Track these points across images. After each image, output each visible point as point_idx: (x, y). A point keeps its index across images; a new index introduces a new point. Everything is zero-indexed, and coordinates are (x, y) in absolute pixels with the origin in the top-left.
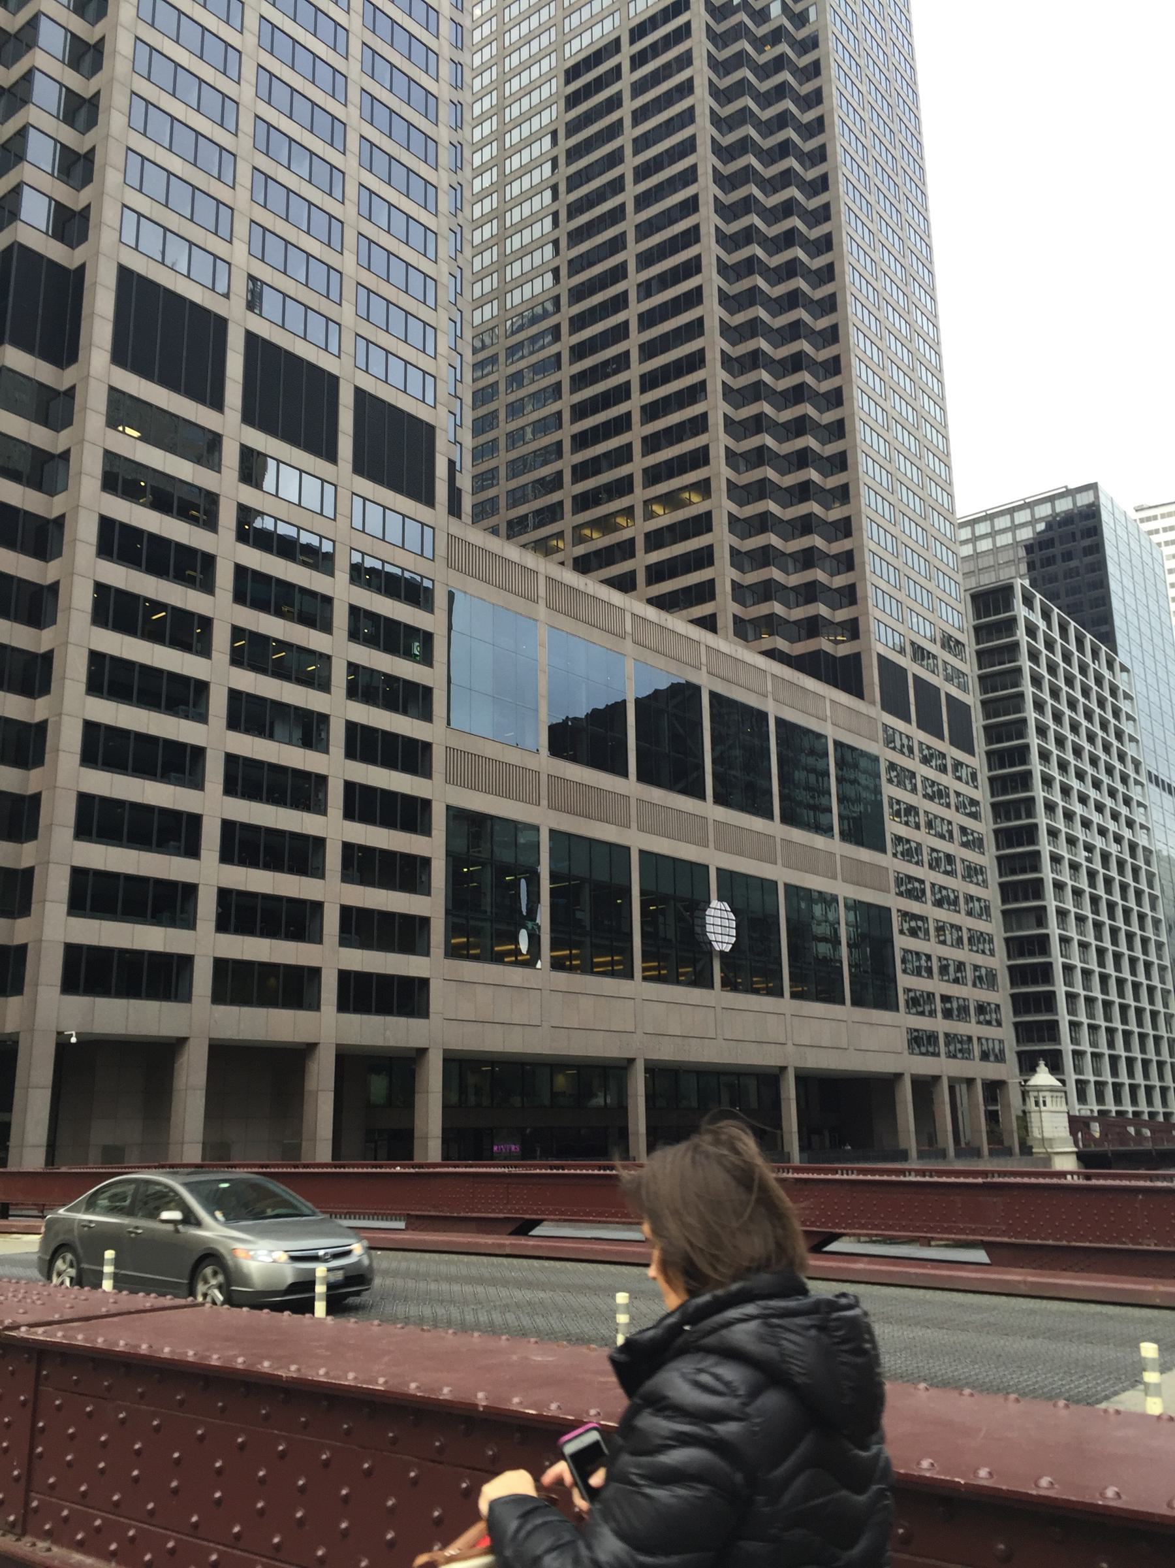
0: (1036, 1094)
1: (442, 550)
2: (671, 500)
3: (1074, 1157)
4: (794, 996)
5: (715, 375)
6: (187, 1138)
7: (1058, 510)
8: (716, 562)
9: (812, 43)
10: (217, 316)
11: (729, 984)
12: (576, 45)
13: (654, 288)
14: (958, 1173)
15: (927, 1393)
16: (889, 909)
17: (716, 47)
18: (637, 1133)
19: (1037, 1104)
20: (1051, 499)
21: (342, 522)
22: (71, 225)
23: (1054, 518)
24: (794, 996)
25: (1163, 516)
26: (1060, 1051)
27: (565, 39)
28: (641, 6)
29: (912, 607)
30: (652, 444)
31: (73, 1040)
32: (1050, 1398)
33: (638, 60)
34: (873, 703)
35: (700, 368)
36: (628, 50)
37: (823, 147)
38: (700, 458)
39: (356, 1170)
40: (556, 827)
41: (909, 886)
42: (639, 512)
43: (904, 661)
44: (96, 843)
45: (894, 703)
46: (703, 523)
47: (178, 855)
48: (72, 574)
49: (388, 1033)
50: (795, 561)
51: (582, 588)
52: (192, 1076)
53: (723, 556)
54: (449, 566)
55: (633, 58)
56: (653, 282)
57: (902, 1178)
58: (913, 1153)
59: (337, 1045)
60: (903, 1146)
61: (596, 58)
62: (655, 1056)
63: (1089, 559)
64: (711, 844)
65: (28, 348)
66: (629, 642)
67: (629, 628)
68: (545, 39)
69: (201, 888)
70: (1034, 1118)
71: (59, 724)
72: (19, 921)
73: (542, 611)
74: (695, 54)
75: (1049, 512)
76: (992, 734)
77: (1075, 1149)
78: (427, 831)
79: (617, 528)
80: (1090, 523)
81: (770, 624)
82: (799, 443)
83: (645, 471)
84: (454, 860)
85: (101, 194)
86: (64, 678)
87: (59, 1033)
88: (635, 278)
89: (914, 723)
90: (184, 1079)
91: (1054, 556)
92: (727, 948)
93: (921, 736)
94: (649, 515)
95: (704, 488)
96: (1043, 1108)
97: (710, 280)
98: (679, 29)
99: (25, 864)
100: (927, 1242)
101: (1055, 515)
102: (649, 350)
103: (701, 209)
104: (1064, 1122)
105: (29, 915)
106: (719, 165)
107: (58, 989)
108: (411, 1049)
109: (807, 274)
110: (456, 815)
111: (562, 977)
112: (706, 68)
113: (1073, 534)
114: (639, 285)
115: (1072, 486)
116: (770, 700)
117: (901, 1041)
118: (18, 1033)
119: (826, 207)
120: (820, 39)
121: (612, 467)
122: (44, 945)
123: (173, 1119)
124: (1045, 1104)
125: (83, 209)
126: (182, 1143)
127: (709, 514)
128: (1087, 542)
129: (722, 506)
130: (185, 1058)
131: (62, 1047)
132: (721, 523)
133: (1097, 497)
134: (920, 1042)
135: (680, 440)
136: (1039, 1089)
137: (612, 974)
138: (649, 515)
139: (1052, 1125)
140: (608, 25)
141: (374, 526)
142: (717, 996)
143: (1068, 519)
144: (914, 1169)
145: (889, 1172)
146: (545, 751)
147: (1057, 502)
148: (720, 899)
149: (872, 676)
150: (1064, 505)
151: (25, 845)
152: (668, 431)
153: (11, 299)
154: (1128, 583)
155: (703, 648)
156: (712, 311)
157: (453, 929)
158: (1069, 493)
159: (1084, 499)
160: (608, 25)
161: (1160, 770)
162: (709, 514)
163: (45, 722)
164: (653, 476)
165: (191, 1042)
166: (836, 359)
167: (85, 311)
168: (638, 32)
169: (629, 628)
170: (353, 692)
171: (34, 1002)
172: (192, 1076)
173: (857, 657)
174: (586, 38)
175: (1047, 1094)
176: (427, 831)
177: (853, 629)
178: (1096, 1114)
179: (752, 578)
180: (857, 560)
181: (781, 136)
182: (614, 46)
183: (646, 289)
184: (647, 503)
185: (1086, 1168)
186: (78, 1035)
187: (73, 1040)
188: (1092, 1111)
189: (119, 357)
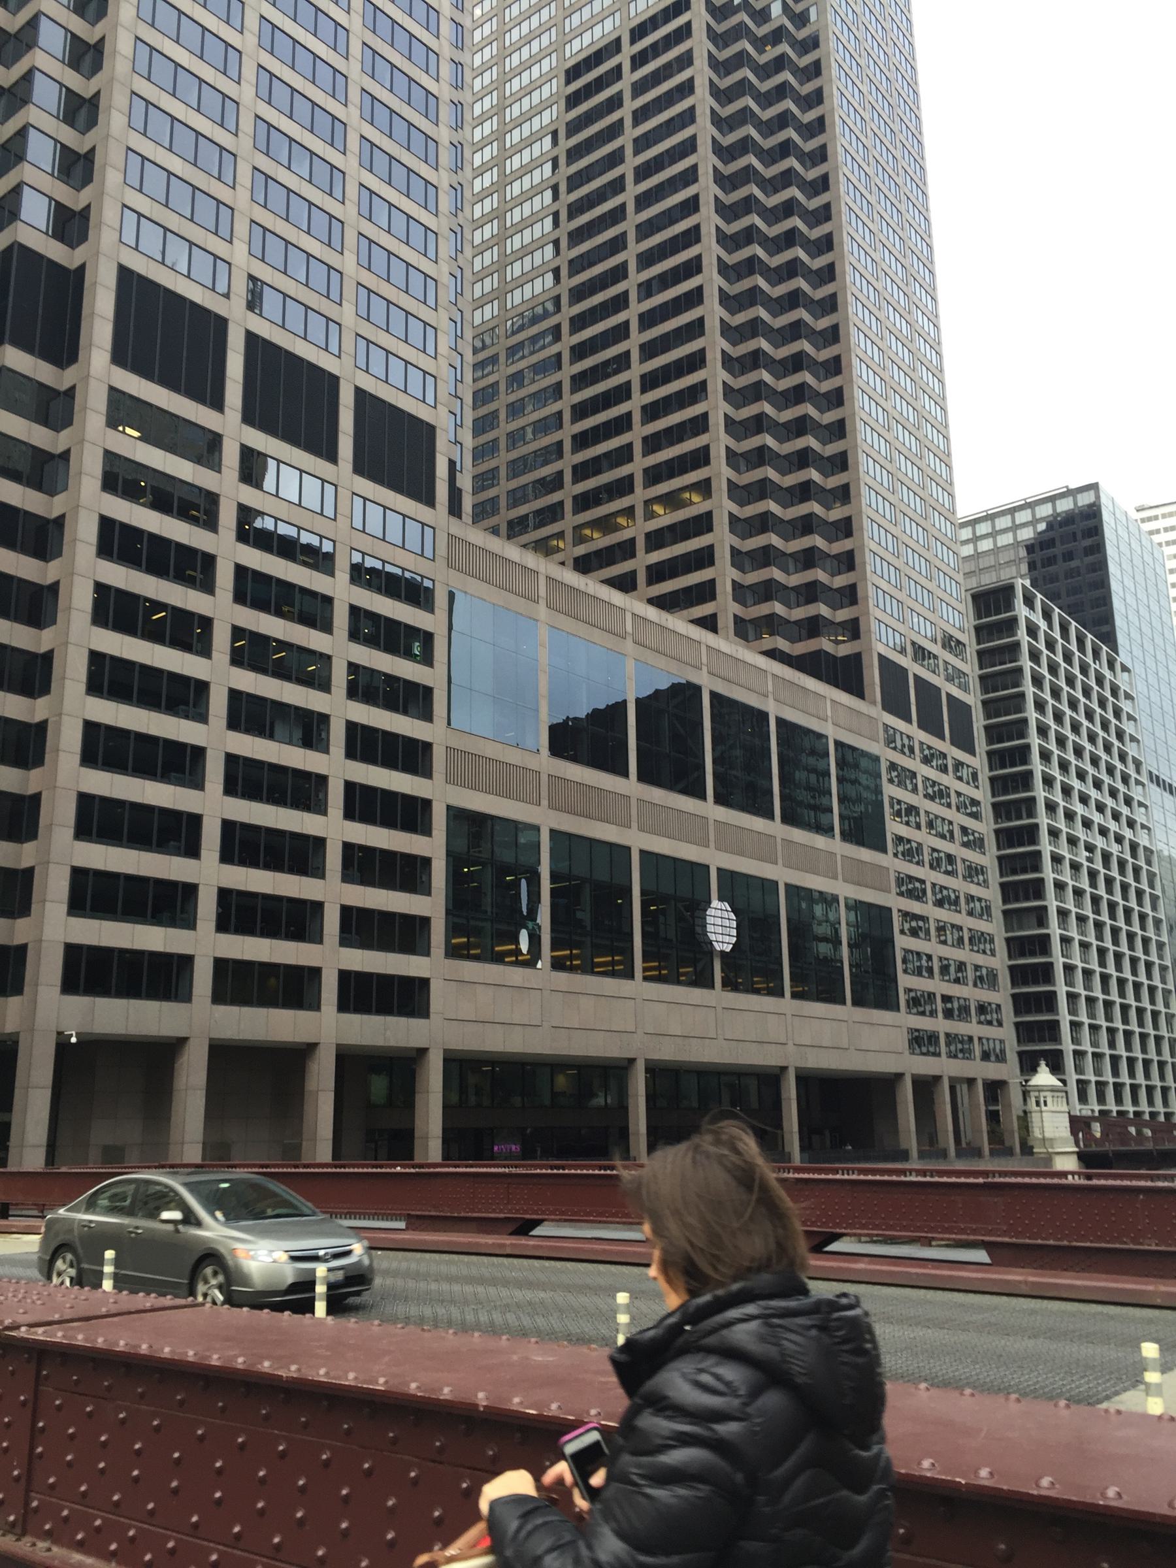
0: (1036, 1094)
1: (442, 550)
2: (672, 500)
3: (1075, 1157)
4: (795, 996)
5: (715, 375)
6: (187, 1138)
7: (1059, 510)
8: (716, 562)
9: (813, 43)
10: (217, 316)
11: (730, 984)
12: (576, 45)
13: (654, 288)
14: (959, 1173)
15: (928, 1393)
16: (890, 909)
17: (717, 47)
18: (637, 1133)
19: (1038, 1104)
20: (1052, 499)
21: (342, 522)
22: (71, 225)
23: (1055, 518)
24: (795, 996)
25: (1164, 516)
26: (1061, 1051)
27: (566, 39)
28: (641, 6)
29: (913, 607)
30: (652, 444)
31: (74, 1040)
32: (1051, 1398)
33: (639, 60)
34: (874, 703)
35: (701, 368)
36: (628, 50)
37: (823, 147)
38: (701, 458)
39: (356, 1170)
40: (556, 827)
41: (910, 886)
42: (639, 512)
43: (905, 661)
44: (96, 843)
45: (895, 703)
46: (703, 523)
47: (178, 855)
48: (73, 574)
49: (388, 1033)
50: (796, 561)
51: (582, 588)
52: (192, 1076)
53: (723, 556)
54: (450, 566)
55: (633, 58)
56: (654, 282)
57: (903, 1178)
58: (914, 1153)
59: (338, 1045)
60: (903, 1146)
61: (597, 58)
62: (656, 1056)
63: (1090, 559)
64: (712, 844)
65: (28, 348)
66: (629, 642)
67: (629, 628)
68: (545, 39)
69: (201, 888)
70: (1035, 1118)
71: (59, 724)
72: (19, 921)
73: (542, 611)
74: (695, 54)
75: (1050, 512)
76: (993, 734)
77: (1076, 1149)
78: (427, 831)
79: (617, 528)
80: (1091, 523)
81: (771, 624)
82: (800, 443)
83: (646, 471)
84: (455, 860)
85: (101, 194)
86: (64, 678)
87: (59, 1033)
88: (635, 278)
89: (915, 723)
90: (184, 1079)
91: (1055, 556)
92: (728, 948)
93: (922, 736)
94: (650, 515)
95: (704, 488)
96: (1044, 1108)
97: (711, 280)
98: (680, 29)
99: (25, 864)
100: (928, 1242)
101: (1055, 515)
102: (649, 350)
103: (701, 209)
104: (1065, 1122)
105: (29, 915)
106: (719, 165)
107: (58, 989)
108: (412, 1049)
109: (808, 274)
110: (456, 815)
111: (562, 977)
112: (707, 68)
113: (1074, 534)
114: (639, 285)
115: (1073, 486)
116: (771, 700)
117: (901, 1041)
118: (18, 1033)
119: (827, 207)
120: (821, 39)
121: (612, 467)
122: (44, 945)
123: (173, 1119)
124: (1046, 1104)
125: (83, 209)
126: (183, 1143)
127: (709, 514)
128: (1087, 542)
129: (723, 506)
130: (185, 1058)
131: (63, 1047)
132: (721, 523)
133: (1098, 497)
134: (921, 1042)
135: (681, 440)
136: (1040, 1089)
137: (613, 974)
138: (650, 515)
139: (1052, 1125)
140: (608, 25)
141: (374, 526)
142: (718, 996)
143: (1069, 519)
144: (914, 1169)
145: (890, 1172)
146: (545, 751)
147: (1058, 502)
148: (721, 899)
149: (873, 676)
150: (1065, 505)
151: (25, 845)
152: (668, 431)
153: (11, 299)
154: (1128, 583)
155: (704, 648)
156: (713, 311)
157: (453, 929)
158: (1070, 493)
159: (1085, 499)
160: (608, 25)
161: (1161, 770)
162: (709, 514)
163: (45, 722)
164: (654, 476)
165: (191, 1042)
166: (837, 359)
167: (85, 311)
168: (639, 32)
169: (629, 628)
170: (353, 692)
171: (34, 1002)
172: (192, 1076)
173: (857, 657)
174: (587, 38)
175: (1048, 1094)
176: (427, 831)
177: (853, 629)
178: (1097, 1114)
179: (753, 578)
180: (857, 560)
181: (781, 136)
182: (615, 46)
183: (647, 289)
184: (648, 503)
185: (1087, 1168)
186: (78, 1035)
187: (74, 1040)
188: (1093, 1111)
189: (119, 357)
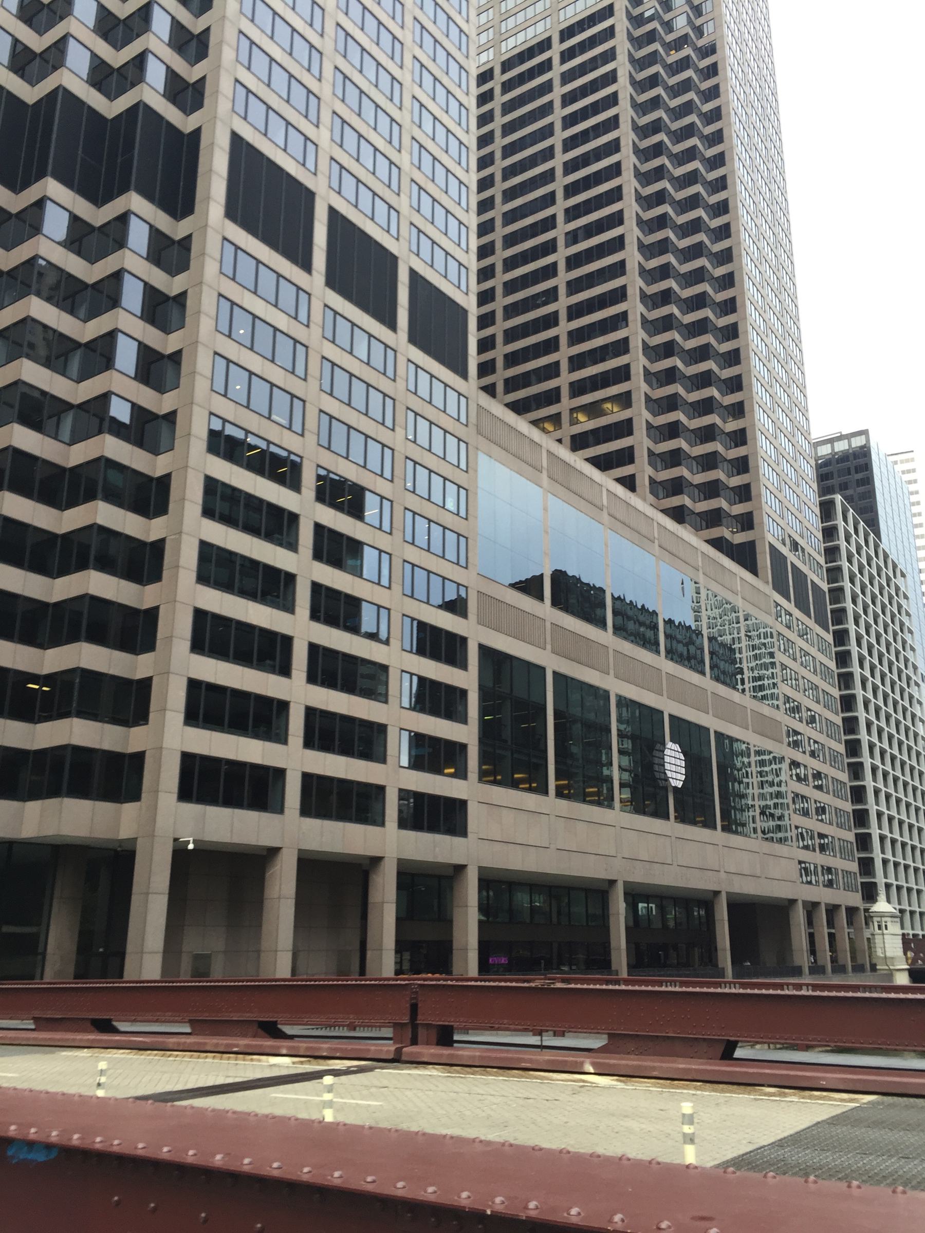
0: (879, 919)
2: (593, 410)
5: (634, 307)
6: (280, 947)
7: (836, 450)
8: (636, 460)
9: (711, 50)
10: (307, 189)
11: (682, 818)
12: (511, 42)
13: (580, 236)
14: (856, 988)
15: (905, 1196)
18: (619, 949)
19: (880, 928)
20: (831, 441)
21: (401, 383)
22: (188, 94)
23: (833, 456)
25: (902, 462)
26: (875, 884)
28: (580, 6)
29: (787, 507)
30: (577, 362)
31: (191, 846)
32: (846, 1177)
33: (567, 56)
35: (622, 302)
36: (557, 48)
37: (720, 131)
39: (509, 984)
40: (557, 670)
41: (795, 738)
42: (565, 418)
43: (785, 551)
44: (209, 656)
45: (780, 586)
47: (273, 672)
48: (192, 403)
49: (437, 849)
51: (572, 463)
52: (283, 883)
53: (641, 456)
55: (503, 84)
56: (579, 232)
57: (779, 992)
59: (399, 860)
60: (797, 962)
62: (631, 879)
63: (861, 489)
66: (605, 514)
69: (292, 705)
70: (878, 939)
71: (178, 543)
72: (135, 730)
75: (830, 451)
77: (907, 967)
79: (602, 413)
80: (861, 461)
82: (703, 367)
83: (572, 384)
87: (176, 840)
88: (562, 228)
89: (793, 602)
90: (277, 888)
91: (833, 486)
92: (679, 784)
94: (574, 422)
95: (625, 400)
96: (885, 932)
97: (631, 231)
98: (542, 63)
100: (807, 1048)
101: (834, 454)
103: (623, 173)
104: (899, 942)
105: (147, 724)
107: (175, 796)
108: (449, 865)
110: (486, 652)
111: (563, 803)
112: (627, 63)
113: (849, 469)
114: (567, 234)
117: (793, 870)
118: (135, 840)
119: (724, 178)
120: (718, 47)
121: (540, 381)
123: (264, 927)
124: (886, 929)
125: (197, 81)
126: (276, 951)
127: (630, 421)
128: (860, 476)
129: (641, 415)
130: (278, 867)
131: (180, 854)
133: (868, 440)
135: (603, 360)
136: (882, 915)
137: (599, 803)
138: (574, 422)
139: (890, 946)
140: (540, 27)
141: (423, 391)
142: (670, 827)
143: (845, 457)
144: (804, 986)
147: (836, 444)
148: (673, 740)
149: (765, 561)
150: (841, 446)
151: (141, 657)
152: (592, 352)
154: (889, 510)
156: (632, 256)
157: (484, 757)
159: (858, 442)
160: (540, 27)
162: (630, 421)
163: (162, 541)
164: (578, 389)
165: (284, 851)
167: (201, 169)
168: (567, 33)
171: (154, 808)
172: (283, 883)
174: (521, 37)
175: (888, 919)
177: (747, 522)
182: (545, 45)
184: (572, 410)
185: (914, 982)
186: (194, 841)
187: (191, 846)
189: (231, 213)
